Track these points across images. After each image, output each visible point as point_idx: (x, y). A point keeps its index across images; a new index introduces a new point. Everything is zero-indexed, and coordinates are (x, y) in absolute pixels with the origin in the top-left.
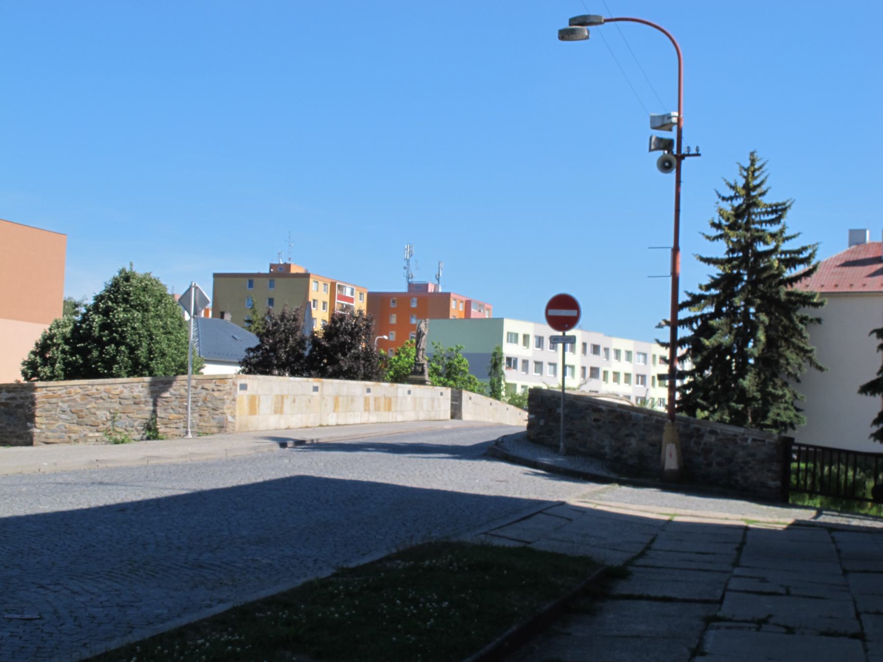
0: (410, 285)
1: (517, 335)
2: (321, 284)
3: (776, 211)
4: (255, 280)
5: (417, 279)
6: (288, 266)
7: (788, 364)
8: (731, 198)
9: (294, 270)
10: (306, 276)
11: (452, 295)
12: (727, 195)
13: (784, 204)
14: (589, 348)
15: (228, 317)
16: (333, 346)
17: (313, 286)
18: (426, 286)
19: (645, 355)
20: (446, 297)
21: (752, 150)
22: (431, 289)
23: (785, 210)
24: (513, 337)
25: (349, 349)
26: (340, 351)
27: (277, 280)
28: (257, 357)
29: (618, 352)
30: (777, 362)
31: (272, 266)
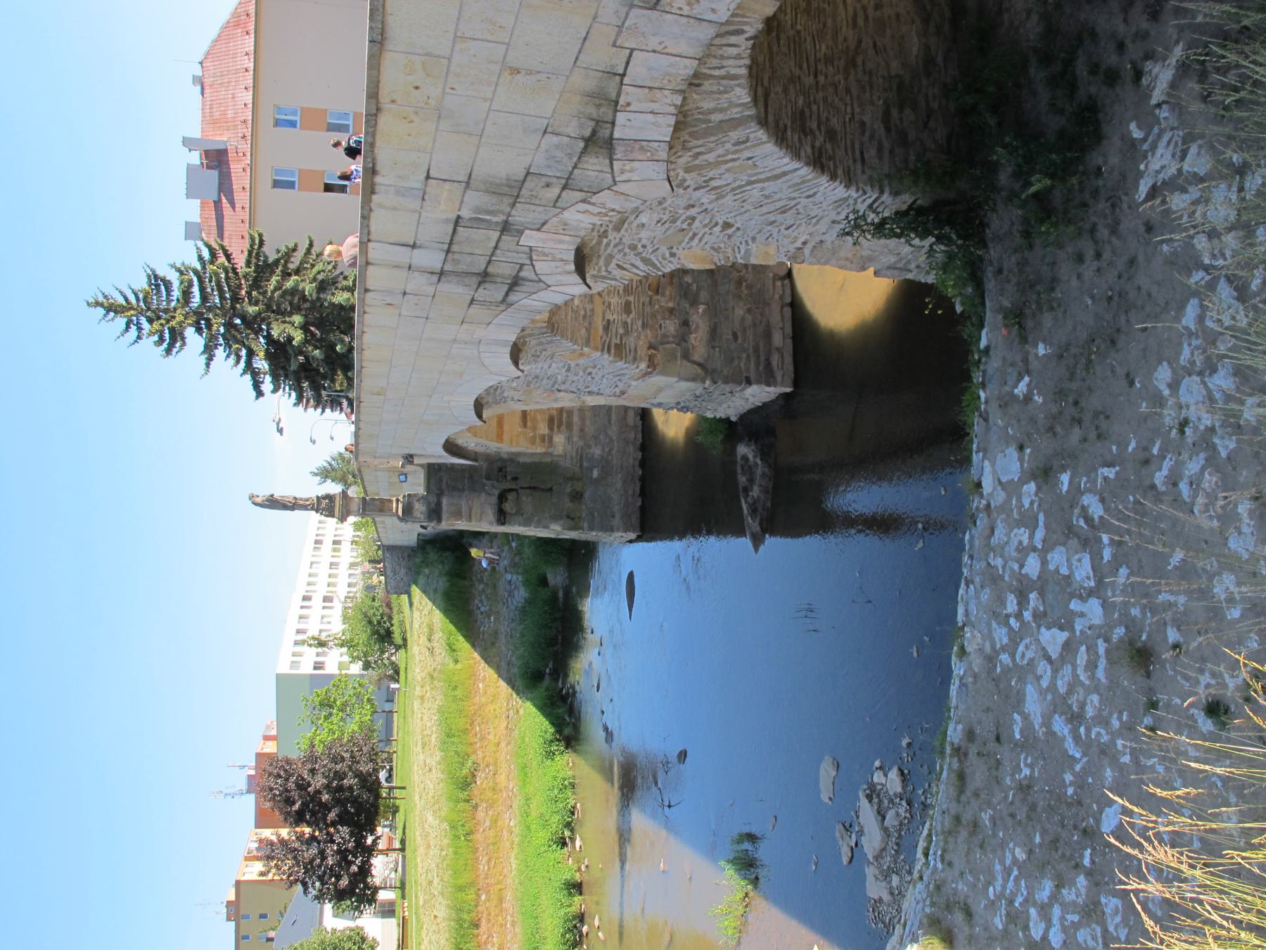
0: (249, 791)
1: (292, 662)
2: (246, 870)
3: (158, 286)
4: (242, 933)
5: (243, 785)
6: (229, 903)
7: (323, 271)
8: (140, 329)
9: (232, 897)
10: (238, 883)
11: (259, 751)
12: (136, 334)
13: (149, 276)
14: (306, 603)
15: (272, 934)
16: (300, 797)
17: (247, 877)
18: (249, 776)
19: (312, 563)
20: (260, 756)
21: (85, 304)
22: (253, 772)
23: (156, 277)
24: (294, 664)
25: (303, 779)
26: (306, 789)
27: (242, 912)
28: (314, 883)
29: (309, 584)
30: (322, 281)
31: (229, 919)
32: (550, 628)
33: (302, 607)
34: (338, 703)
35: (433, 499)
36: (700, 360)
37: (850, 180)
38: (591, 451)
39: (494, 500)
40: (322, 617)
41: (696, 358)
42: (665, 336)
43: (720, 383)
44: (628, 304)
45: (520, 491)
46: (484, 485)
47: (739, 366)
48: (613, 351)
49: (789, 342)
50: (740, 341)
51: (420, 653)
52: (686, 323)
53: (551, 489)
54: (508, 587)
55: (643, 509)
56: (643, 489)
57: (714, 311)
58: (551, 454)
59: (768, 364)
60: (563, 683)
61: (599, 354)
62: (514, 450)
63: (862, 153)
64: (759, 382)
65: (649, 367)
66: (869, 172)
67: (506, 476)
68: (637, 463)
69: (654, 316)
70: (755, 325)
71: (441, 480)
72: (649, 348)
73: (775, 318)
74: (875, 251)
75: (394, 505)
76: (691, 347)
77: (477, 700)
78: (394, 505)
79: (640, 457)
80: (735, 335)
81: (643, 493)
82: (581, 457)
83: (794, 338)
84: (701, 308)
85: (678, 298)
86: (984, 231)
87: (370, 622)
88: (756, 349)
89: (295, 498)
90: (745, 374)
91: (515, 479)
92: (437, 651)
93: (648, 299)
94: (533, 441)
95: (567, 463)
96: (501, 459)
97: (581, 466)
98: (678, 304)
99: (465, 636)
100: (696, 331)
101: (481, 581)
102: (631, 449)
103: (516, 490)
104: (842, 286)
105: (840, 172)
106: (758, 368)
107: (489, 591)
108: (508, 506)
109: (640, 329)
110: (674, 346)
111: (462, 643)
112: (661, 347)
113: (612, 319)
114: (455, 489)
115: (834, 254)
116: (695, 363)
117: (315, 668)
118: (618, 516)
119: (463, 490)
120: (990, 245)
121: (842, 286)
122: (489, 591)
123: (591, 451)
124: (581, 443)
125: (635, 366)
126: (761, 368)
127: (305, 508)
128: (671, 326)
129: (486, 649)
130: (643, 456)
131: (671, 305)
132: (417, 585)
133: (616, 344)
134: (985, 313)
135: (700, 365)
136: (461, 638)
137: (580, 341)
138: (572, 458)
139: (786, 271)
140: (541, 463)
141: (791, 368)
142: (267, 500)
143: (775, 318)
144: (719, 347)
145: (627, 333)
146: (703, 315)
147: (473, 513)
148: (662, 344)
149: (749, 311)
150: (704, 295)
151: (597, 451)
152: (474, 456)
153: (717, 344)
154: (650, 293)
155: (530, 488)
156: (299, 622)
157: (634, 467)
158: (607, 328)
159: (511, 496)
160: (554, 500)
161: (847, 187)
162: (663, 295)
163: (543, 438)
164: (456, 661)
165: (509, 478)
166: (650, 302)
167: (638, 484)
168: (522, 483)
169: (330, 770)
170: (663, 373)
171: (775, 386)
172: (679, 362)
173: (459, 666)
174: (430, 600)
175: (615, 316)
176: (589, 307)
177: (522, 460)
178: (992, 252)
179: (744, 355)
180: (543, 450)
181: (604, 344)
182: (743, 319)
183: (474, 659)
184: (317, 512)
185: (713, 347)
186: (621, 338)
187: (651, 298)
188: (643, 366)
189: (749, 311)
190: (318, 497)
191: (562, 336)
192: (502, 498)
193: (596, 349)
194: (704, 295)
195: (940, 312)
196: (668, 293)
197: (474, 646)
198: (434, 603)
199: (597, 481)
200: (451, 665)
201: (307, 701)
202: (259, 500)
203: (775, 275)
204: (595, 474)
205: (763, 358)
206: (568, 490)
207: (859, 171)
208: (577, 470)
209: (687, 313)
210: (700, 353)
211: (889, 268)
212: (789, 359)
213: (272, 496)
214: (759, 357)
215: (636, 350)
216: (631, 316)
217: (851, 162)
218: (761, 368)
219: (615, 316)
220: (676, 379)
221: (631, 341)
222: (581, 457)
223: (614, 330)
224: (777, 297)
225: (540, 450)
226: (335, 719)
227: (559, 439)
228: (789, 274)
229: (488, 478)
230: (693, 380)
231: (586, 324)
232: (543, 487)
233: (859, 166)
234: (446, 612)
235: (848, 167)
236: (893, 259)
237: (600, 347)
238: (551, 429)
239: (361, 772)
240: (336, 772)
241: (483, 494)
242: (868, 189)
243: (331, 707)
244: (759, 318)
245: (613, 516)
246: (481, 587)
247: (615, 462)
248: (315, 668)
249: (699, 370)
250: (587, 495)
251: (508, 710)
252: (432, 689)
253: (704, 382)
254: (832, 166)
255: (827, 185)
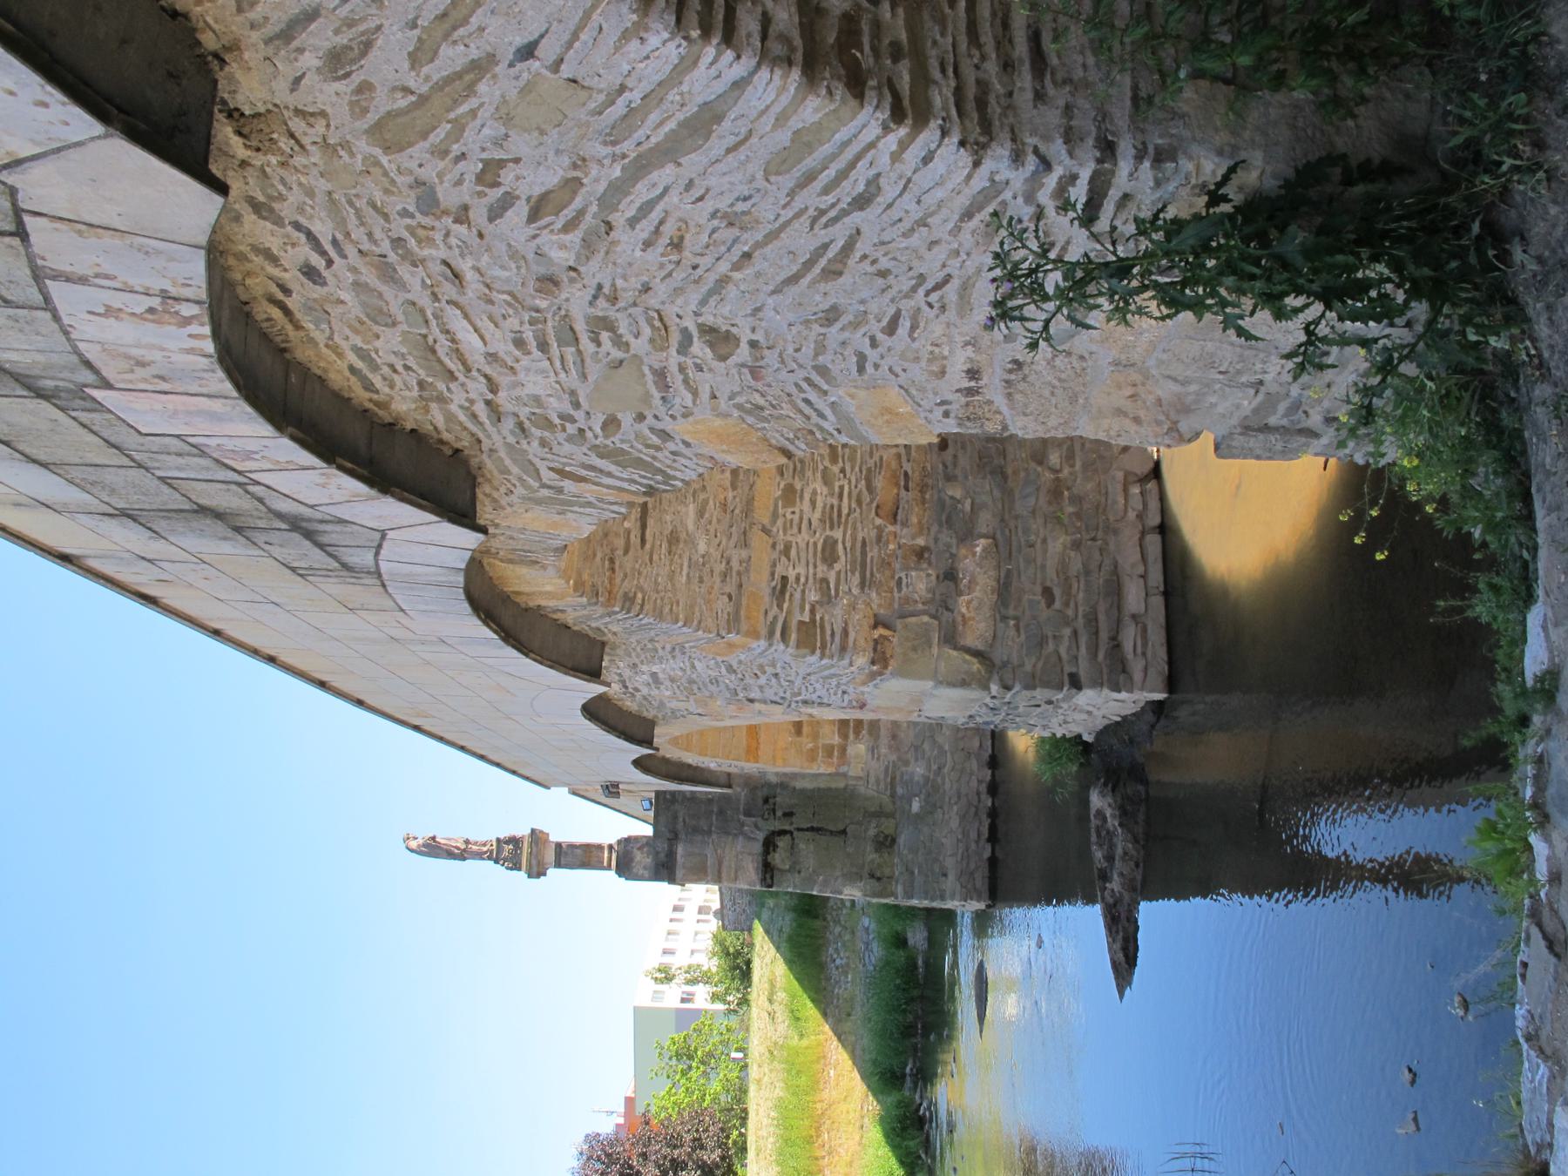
14: (677, 915)
25: (631, 1167)
32: (904, 1011)
33: (671, 920)
34: (699, 1053)
35: (663, 846)
36: (979, 645)
37: (986, 126)
38: (910, 769)
39: (758, 847)
40: (696, 934)
41: (970, 640)
42: (907, 600)
43: (1017, 688)
44: (830, 545)
45: (795, 833)
46: (743, 825)
47: (1057, 652)
48: (794, 636)
49: (1158, 602)
50: (1057, 605)
51: (759, 1018)
52: (950, 576)
53: (844, 832)
54: (865, 936)
55: (993, 862)
56: (993, 829)
57: (1004, 549)
58: (844, 775)
59: (1116, 646)
60: (921, 1097)
61: (763, 643)
62: (788, 770)
63: (1035, 38)
64: (1097, 684)
65: (873, 663)
66: (1059, 96)
67: (774, 811)
68: (983, 788)
69: (885, 564)
70: (1087, 573)
71: (675, 817)
72: (875, 626)
73: (1129, 557)
74: (1185, 382)
75: (606, 855)
76: (959, 619)
77: (825, 1095)
78: (606, 855)
79: (989, 778)
80: (1048, 593)
81: (993, 838)
82: (893, 779)
83: (1166, 594)
84: (981, 545)
85: (935, 528)
86: (1505, 256)
87: (728, 954)
88: (1092, 620)
89: (467, 842)
90: (1068, 669)
91: (788, 815)
92: (780, 1016)
93: (873, 533)
94: (812, 756)
95: (867, 791)
96: (769, 785)
97: (893, 795)
98: (936, 540)
99: (813, 1001)
100: (970, 589)
101: (837, 922)
102: (974, 764)
103: (791, 833)
104: (1238, 487)
105: (941, 97)
106: (1096, 655)
107: (847, 937)
108: (779, 858)
109: (855, 591)
110: (926, 619)
111: (810, 1011)
112: (899, 624)
113: (791, 574)
114: (696, 830)
115: (1073, 399)
116: (968, 651)
117: (683, 1000)
118: (951, 877)
119: (709, 833)
120: (1535, 307)
121: (1238, 487)
122: (847, 937)
123: (910, 769)
124: (893, 757)
125: (846, 662)
126: (1101, 656)
127: (479, 856)
128: (920, 583)
129: (840, 1021)
130: (993, 775)
131: (921, 542)
132: (760, 920)
133: (801, 623)
134: (1534, 549)
135: (977, 654)
136: (810, 1004)
137: (710, 622)
138: (878, 782)
139: (1151, 465)
140: (830, 789)
141: (1162, 653)
142: (424, 846)
143: (1129, 557)
144: (1016, 618)
145: (828, 598)
146: (983, 558)
147: (724, 870)
148: (902, 616)
149: (1076, 545)
150: (985, 521)
151: (918, 770)
152: (728, 781)
153: (1011, 612)
154: (878, 521)
155: (812, 829)
156: (667, 940)
157: (978, 794)
158: (781, 589)
159: (782, 843)
160: (850, 850)
161: (977, 148)
162: (905, 524)
163: (829, 751)
164: (801, 1036)
165: (779, 813)
166: (879, 539)
167: (986, 822)
168: (800, 821)
169: (665, 1157)
170: (901, 673)
171: (1130, 691)
172: (935, 650)
173: (805, 1042)
174: (773, 942)
175: (801, 570)
176: (737, 555)
177: (799, 785)
178: (1542, 329)
179: (1067, 632)
180: (831, 770)
181: (773, 623)
182: (1063, 567)
183: (824, 1033)
184: (496, 862)
185: (1004, 618)
186: (813, 611)
187: (880, 529)
188: (862, 661)
189: (1076, 545)
190: (498, 840)
191: (660, 616)
192: (769, 845)
193: (755, 634)
194: (985, 521)
195: (1379, 557)
196: (914, 520)
197: (825, 1015)
198: (778, 948)
199: (919, 818)
200: (795, 1041)
201: (662, 1048)
202: (413, 844)
203: (1127, 474)
204: (916, 806)
205: (1104, 636)
206: (872, 832)
207: (1024, 98)
208: (886, 799)
209: (953, 556)
210: (976, 632)
211: (1247, 429)
212: (1157, 637)
213: (433, 838)
214: (1097, 633)
215: (845, 632)
216: (837, 566)
217: (992, 68)
218: (1101, 656)
219: (801, 570)
220: (931, 684)
221: (835, 617)
222: (893, 779)
223: (798, 595)
224: (1132, 515)
225: (823, 769)
226: (694, 1074)
227: (859, 749)
228: (1156, 472)
229: (748, 814)
230: (964, 684)
231: (730, 588)
232: (831, 827)
233: (1025, 80)
234: (790, 963)
235: (983, 85)
236: (1247, 403)
237: (764, 632)
238: (845, 736)
239: (705, 1163)
240: (673, 1160)
241: (741, 838)
242: (1056, 149)
243: (691, 1058)
244: (1097, 555)
245: (945, 875)
246: (838, 929)
247: (947, 786)
248: (683, 1000)
249: (976, 665)
250: (901, 840)
251: (863, 1117)
252: (771, 1071)
253: (986, 688)
254: (905, 82)
255: (891, 142)
